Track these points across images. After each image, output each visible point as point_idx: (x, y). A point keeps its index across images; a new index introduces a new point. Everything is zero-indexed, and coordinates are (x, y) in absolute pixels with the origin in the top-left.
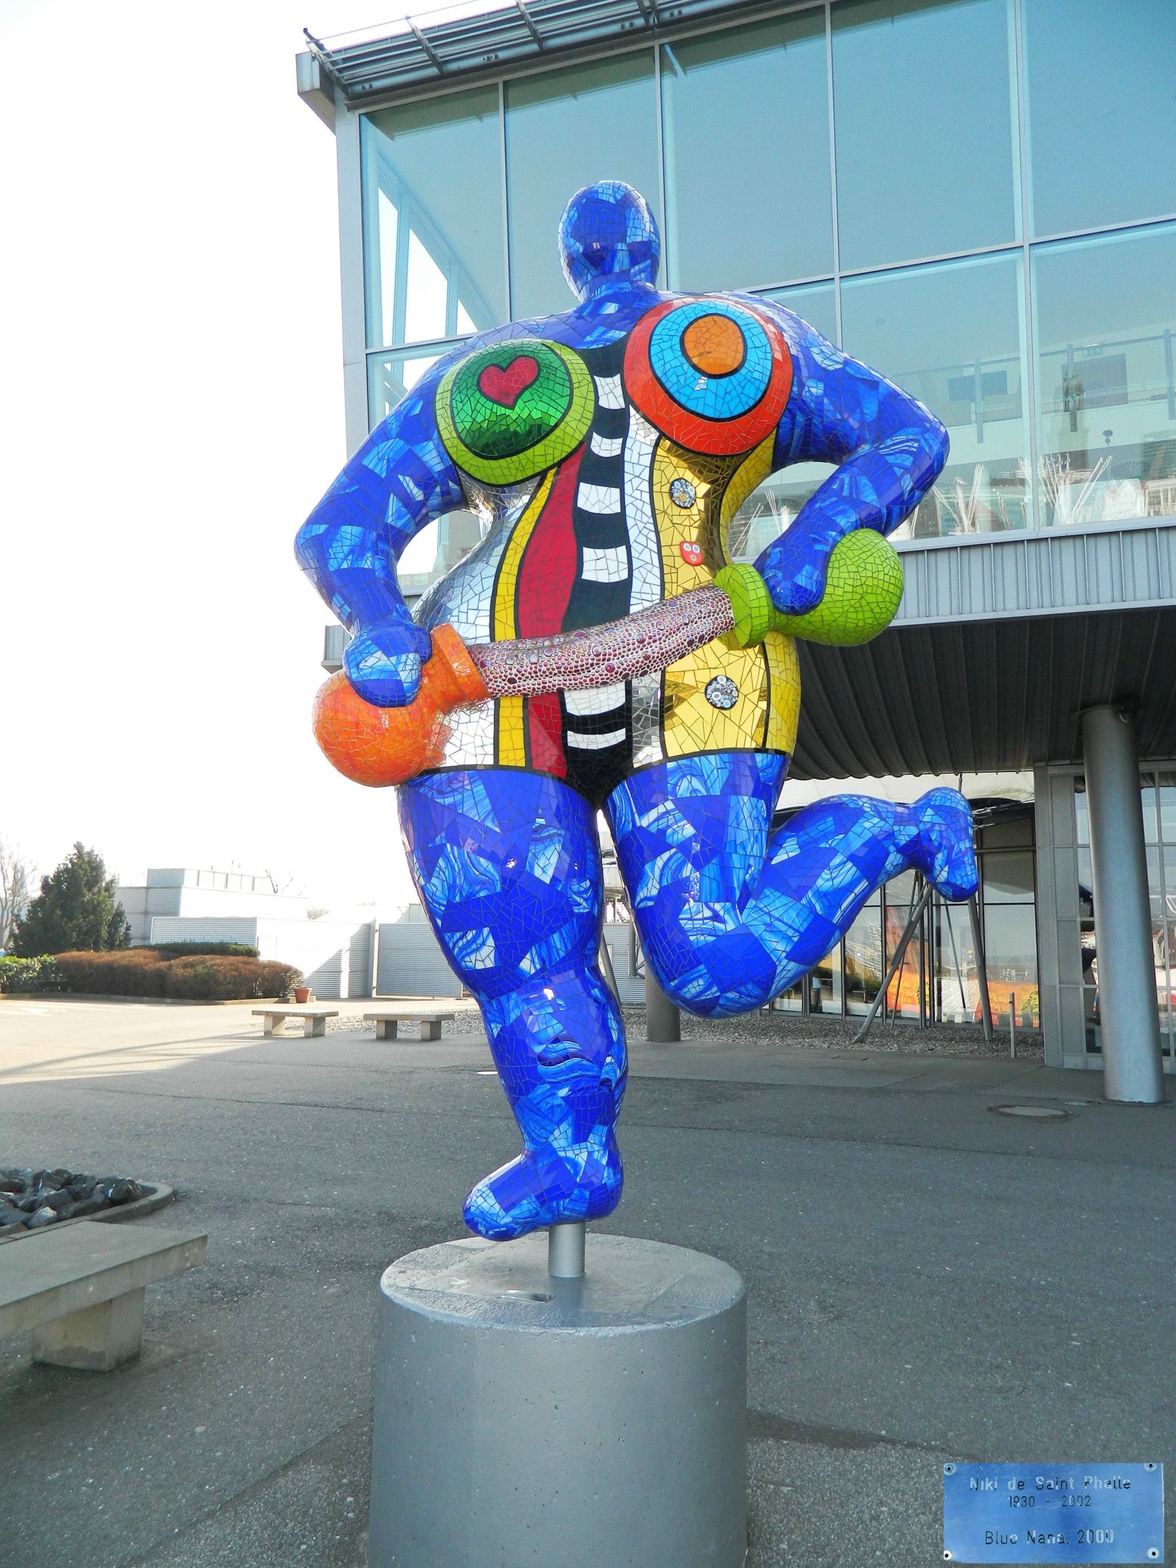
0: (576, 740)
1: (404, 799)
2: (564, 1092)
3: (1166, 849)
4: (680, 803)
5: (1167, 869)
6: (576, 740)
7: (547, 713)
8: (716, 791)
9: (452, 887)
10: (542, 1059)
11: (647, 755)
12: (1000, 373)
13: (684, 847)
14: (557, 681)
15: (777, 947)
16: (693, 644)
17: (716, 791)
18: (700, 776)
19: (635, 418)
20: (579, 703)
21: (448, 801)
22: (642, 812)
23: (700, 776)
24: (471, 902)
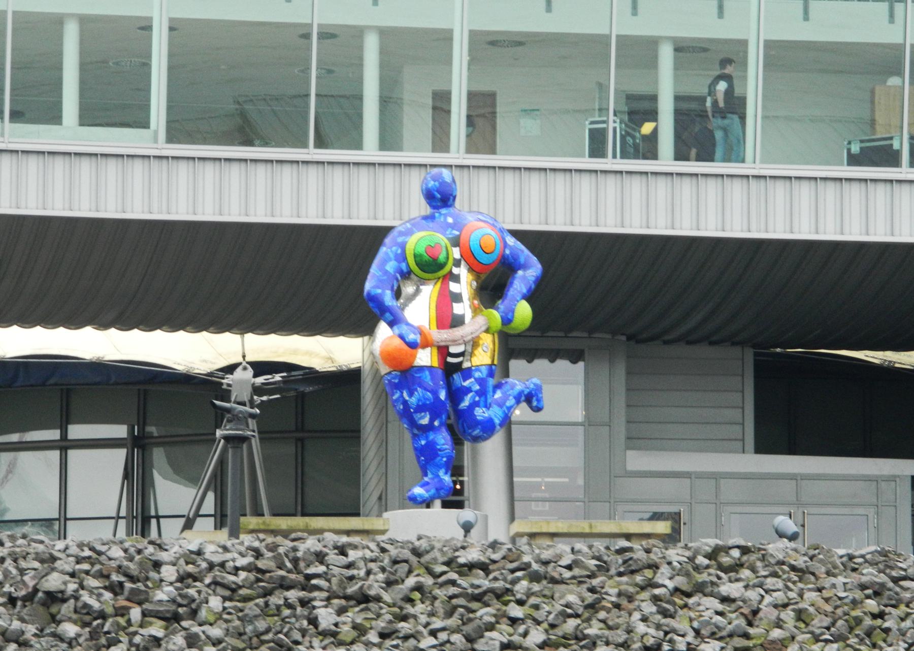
0: (450, 359)
1: (317, 372)
2: (445, 459)
3: (161, 520)
4: (476, 379)
5: (516, 449)
6: (450, 359)
7: (443, 351)
8: (485, 376)
9: (419, 400)
10: (440, 450)
11: (466, 365)
12: (470, 36)
13: (476, 392)
14: (448, 343)
15: (497, 421)
16: (736, 440)
17: (485, 376)
18: (481, 371)
19: (463, 262)
20: (453, 350)
21: (418, 375)
22: (464, 380)
23: (481, 371)
24: (424, 405)
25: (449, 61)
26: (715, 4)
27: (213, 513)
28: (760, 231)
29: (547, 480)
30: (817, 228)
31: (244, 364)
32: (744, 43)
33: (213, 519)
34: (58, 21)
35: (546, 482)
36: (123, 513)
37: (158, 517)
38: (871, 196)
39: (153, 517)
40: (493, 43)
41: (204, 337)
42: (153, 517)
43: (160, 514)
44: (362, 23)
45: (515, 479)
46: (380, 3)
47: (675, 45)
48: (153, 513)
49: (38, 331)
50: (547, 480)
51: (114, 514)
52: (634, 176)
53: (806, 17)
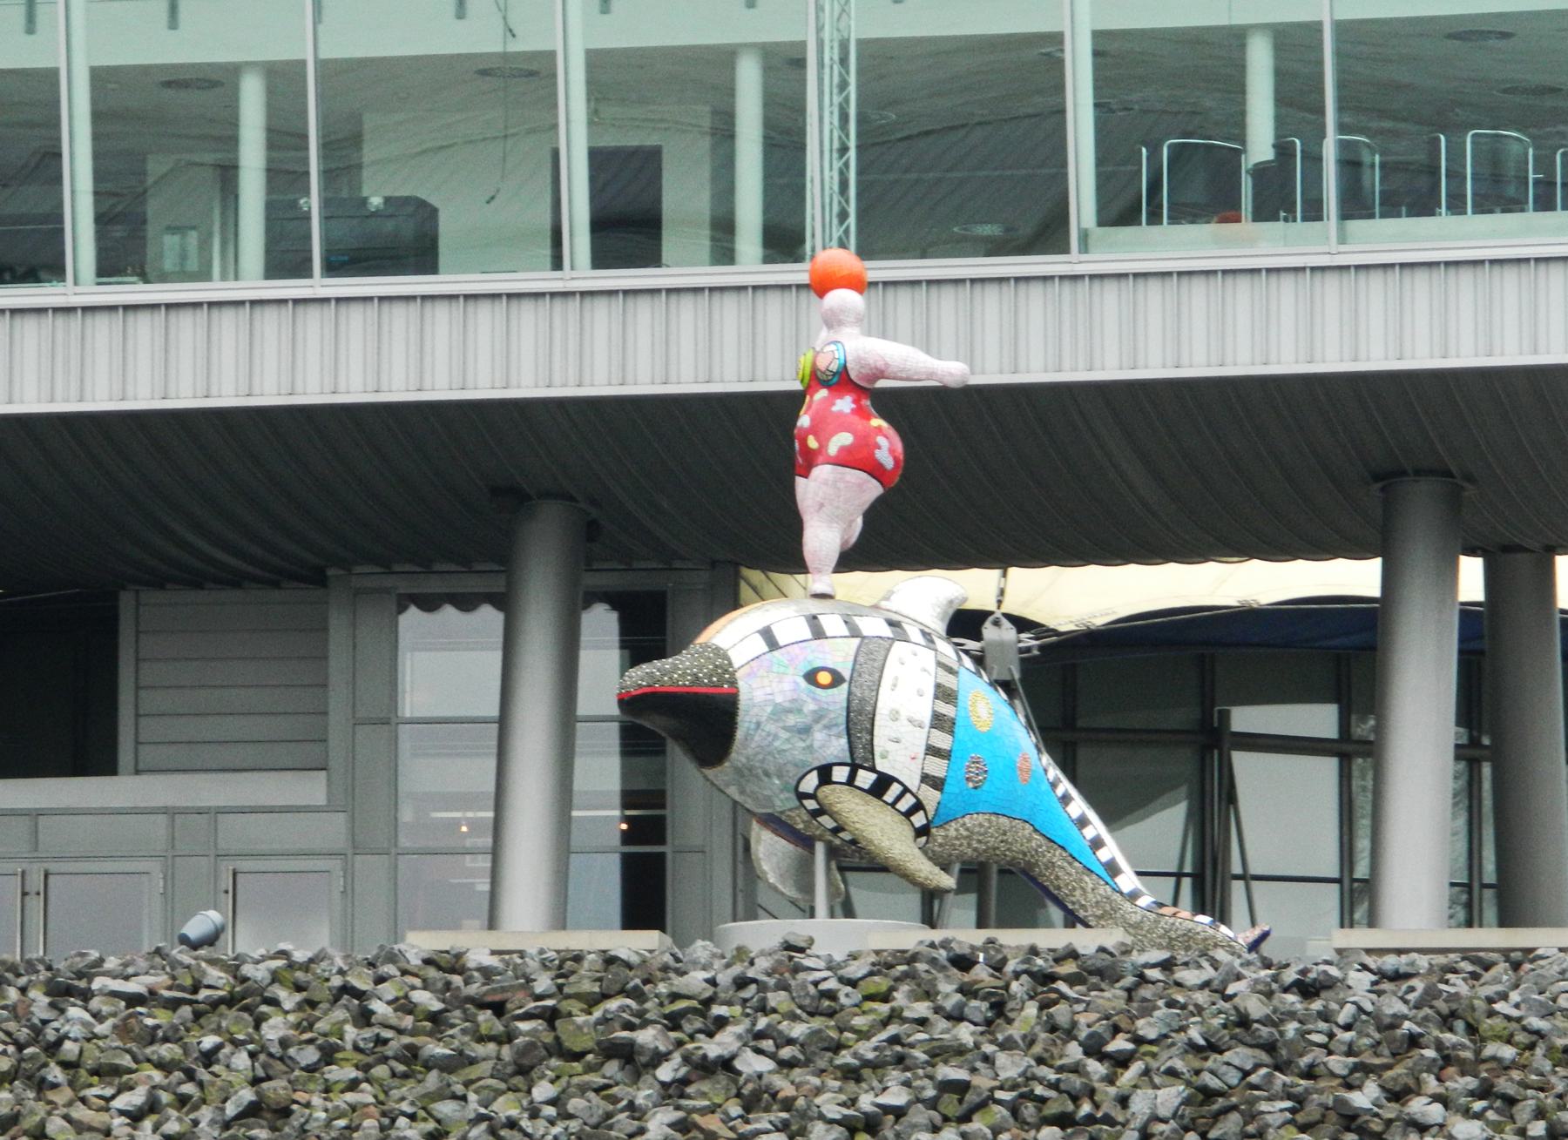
3: (1255, 884)
25: (97, 116)
26: (164, 6)
27: (1335, 874)
28: (1076, 370)
29: (470, 814)
30: (1016, 366)
31: (998, 614)
32: (1320, 23)
33: (1336, 886)
34: (1237, 37)
35: (467, 819)
36: (1188, 869)
37: (1244, 877)
38: (934, 307)
39: (1237, 877)
40: (484, 73)
41: (1133, 571)
42: (1237, 877)
43: (1255, 869)
44: (1239, 19)
45: (491, 814)
46: (616, 5)
47: (1275, 38)
48: (1237, 869)
49: (1300, 565)
50: (470, 814)
51: (1174, 869)
52: (1106, 282)
53: (31, 26)
